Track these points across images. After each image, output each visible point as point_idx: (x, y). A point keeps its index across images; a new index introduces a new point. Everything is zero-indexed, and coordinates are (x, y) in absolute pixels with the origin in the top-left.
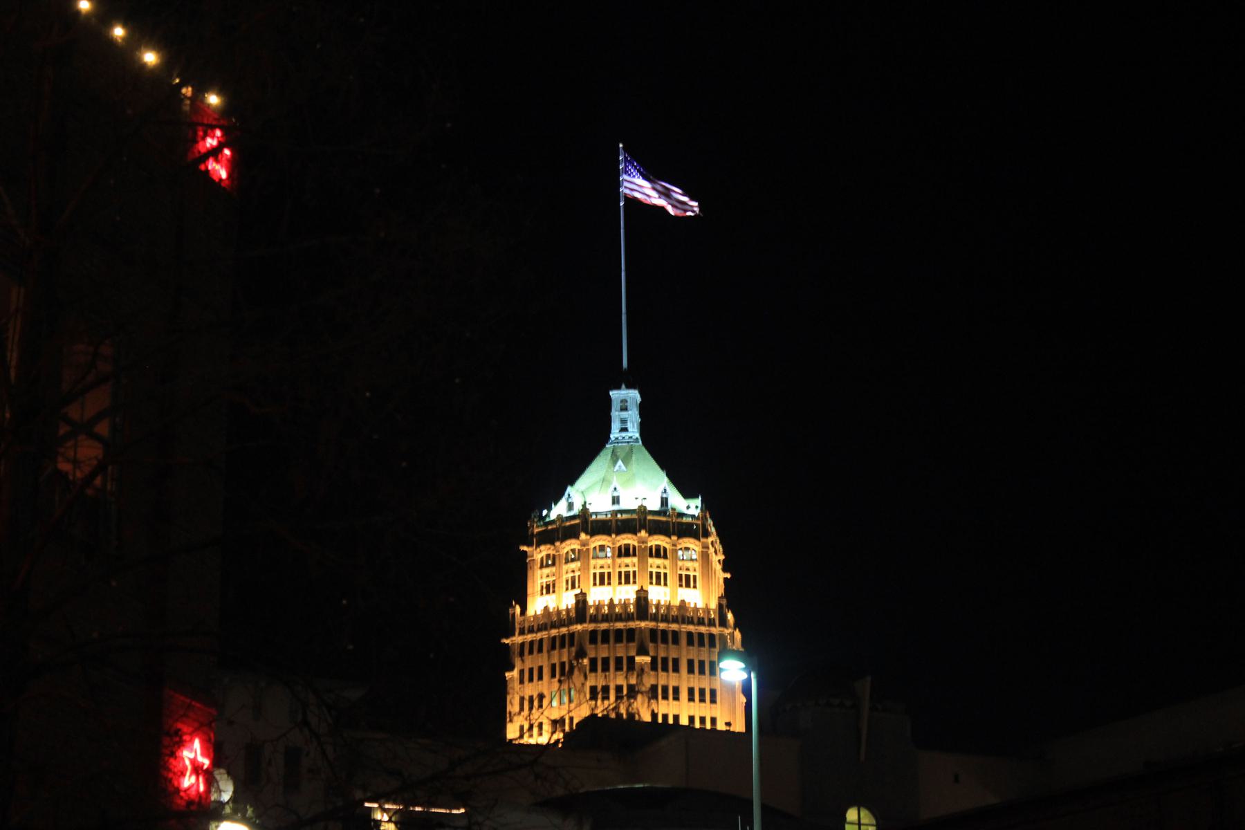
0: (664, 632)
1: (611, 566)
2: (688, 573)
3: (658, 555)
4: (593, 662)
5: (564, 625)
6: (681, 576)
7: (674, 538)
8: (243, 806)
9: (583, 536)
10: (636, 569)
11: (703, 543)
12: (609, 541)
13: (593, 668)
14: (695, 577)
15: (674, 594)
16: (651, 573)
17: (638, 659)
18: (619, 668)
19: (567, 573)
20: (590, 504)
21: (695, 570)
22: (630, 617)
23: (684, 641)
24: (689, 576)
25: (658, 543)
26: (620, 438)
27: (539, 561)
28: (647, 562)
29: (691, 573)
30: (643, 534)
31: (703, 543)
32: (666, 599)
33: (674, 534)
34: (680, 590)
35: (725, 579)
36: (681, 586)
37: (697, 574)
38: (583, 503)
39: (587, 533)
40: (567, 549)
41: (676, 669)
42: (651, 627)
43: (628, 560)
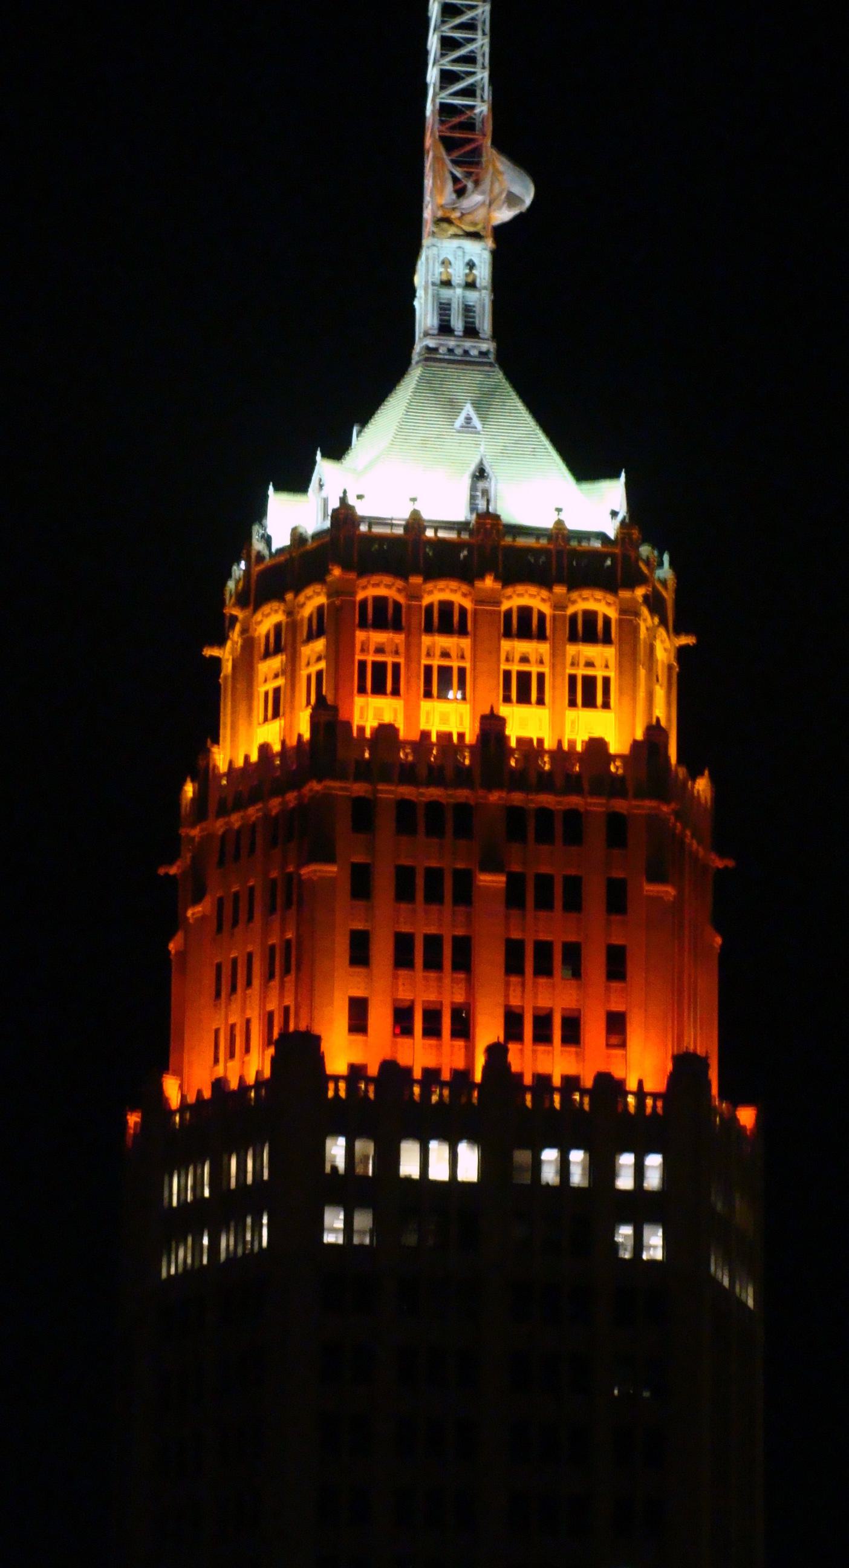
0: (434, 807)
1: (402, 650)
2: (590, 672)
3: (380, 624)
4: (515, 885)
5: (252, 801)
6: (507, 674)
7: (560, 590)
8: (356, 1240)
9: (489, 582)
10: (467, 665)
11: (622, 602)
12: (543, 600)
13: (514, 896)
14: (606, 681)
15: (557, 723)
16: (362, 664)
17: (485, 879)
18: (434, 896)
19: (308, 664)
20: (360, 497)
21: (541, 662)
22: (463, 777)
23: (386, 824)
24: (384, 665)
25: (446, 596)
26: (459, 351)
27: (263, 641)
28: (420, 643)
29: (599, 673)
30: (489, 582)
31: (622, 602)
32: (445, 728)
33: (560, 581)
34: (571, 714)
35: (682, 653)
36: (572, 703)
37: (612, 674)
38: (341, 495)
39: (346, 567)
40: (371, 592)
41: (574, 903)
42: (355, 795)
43: (443, 642)
